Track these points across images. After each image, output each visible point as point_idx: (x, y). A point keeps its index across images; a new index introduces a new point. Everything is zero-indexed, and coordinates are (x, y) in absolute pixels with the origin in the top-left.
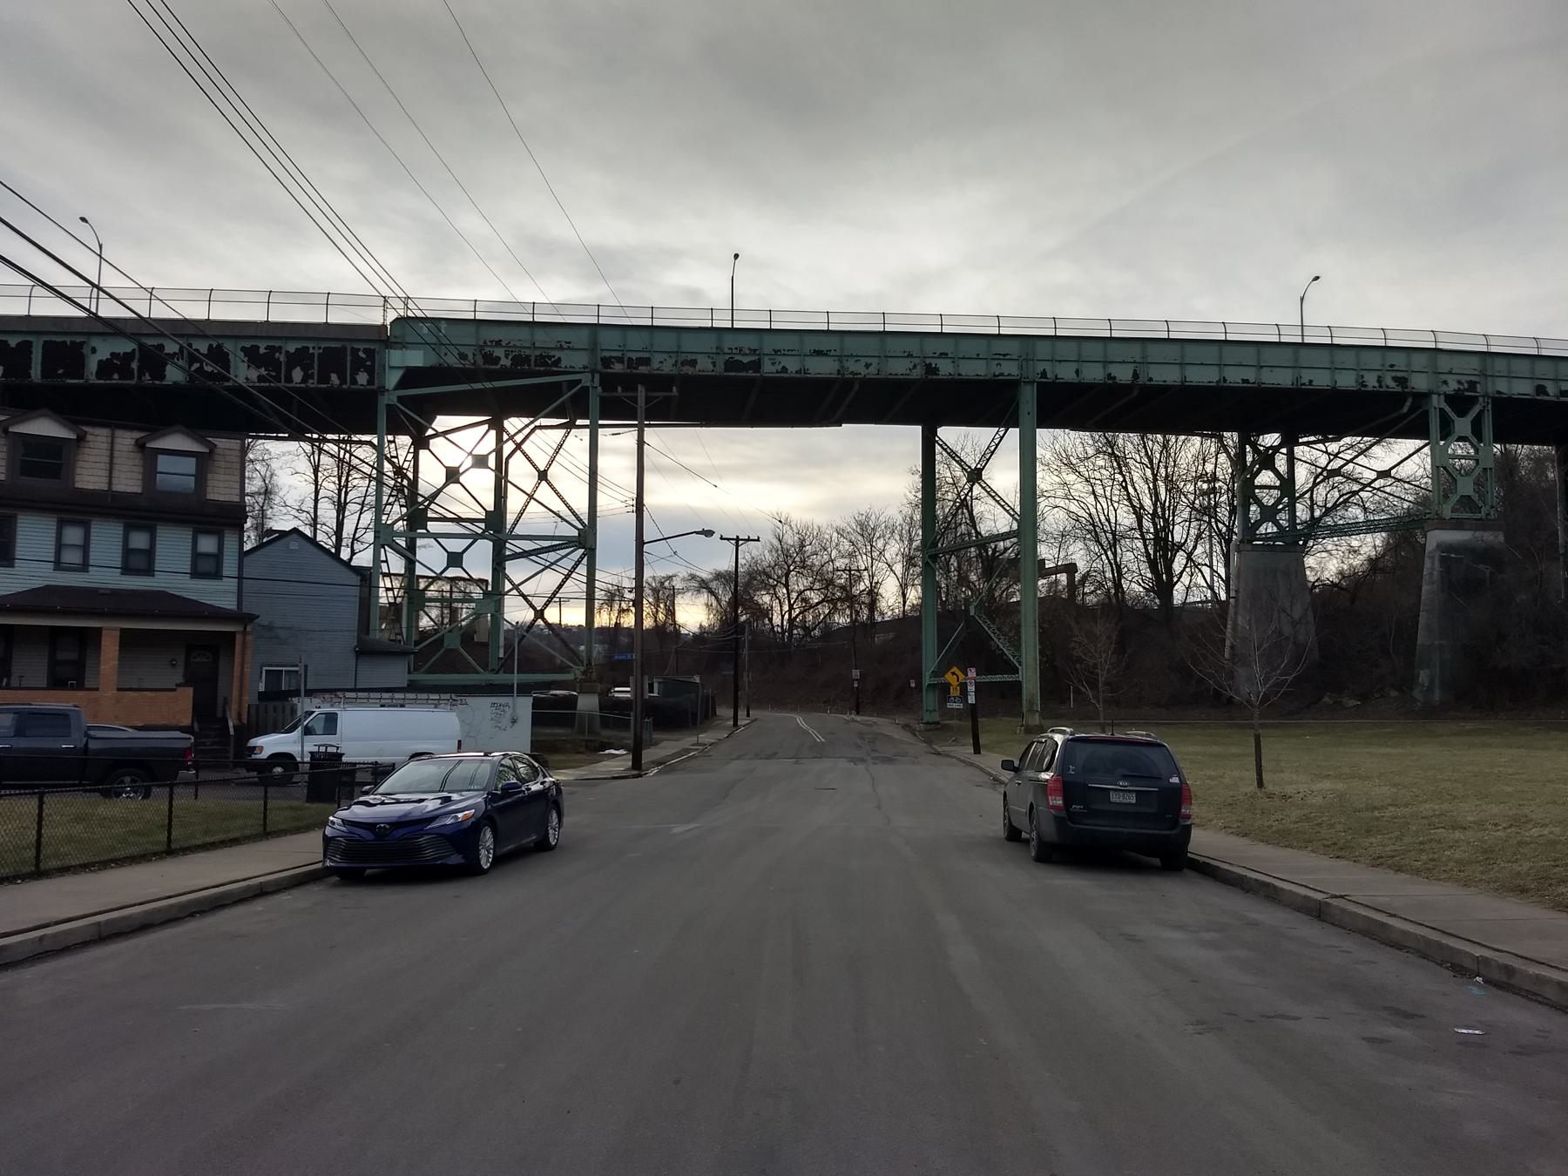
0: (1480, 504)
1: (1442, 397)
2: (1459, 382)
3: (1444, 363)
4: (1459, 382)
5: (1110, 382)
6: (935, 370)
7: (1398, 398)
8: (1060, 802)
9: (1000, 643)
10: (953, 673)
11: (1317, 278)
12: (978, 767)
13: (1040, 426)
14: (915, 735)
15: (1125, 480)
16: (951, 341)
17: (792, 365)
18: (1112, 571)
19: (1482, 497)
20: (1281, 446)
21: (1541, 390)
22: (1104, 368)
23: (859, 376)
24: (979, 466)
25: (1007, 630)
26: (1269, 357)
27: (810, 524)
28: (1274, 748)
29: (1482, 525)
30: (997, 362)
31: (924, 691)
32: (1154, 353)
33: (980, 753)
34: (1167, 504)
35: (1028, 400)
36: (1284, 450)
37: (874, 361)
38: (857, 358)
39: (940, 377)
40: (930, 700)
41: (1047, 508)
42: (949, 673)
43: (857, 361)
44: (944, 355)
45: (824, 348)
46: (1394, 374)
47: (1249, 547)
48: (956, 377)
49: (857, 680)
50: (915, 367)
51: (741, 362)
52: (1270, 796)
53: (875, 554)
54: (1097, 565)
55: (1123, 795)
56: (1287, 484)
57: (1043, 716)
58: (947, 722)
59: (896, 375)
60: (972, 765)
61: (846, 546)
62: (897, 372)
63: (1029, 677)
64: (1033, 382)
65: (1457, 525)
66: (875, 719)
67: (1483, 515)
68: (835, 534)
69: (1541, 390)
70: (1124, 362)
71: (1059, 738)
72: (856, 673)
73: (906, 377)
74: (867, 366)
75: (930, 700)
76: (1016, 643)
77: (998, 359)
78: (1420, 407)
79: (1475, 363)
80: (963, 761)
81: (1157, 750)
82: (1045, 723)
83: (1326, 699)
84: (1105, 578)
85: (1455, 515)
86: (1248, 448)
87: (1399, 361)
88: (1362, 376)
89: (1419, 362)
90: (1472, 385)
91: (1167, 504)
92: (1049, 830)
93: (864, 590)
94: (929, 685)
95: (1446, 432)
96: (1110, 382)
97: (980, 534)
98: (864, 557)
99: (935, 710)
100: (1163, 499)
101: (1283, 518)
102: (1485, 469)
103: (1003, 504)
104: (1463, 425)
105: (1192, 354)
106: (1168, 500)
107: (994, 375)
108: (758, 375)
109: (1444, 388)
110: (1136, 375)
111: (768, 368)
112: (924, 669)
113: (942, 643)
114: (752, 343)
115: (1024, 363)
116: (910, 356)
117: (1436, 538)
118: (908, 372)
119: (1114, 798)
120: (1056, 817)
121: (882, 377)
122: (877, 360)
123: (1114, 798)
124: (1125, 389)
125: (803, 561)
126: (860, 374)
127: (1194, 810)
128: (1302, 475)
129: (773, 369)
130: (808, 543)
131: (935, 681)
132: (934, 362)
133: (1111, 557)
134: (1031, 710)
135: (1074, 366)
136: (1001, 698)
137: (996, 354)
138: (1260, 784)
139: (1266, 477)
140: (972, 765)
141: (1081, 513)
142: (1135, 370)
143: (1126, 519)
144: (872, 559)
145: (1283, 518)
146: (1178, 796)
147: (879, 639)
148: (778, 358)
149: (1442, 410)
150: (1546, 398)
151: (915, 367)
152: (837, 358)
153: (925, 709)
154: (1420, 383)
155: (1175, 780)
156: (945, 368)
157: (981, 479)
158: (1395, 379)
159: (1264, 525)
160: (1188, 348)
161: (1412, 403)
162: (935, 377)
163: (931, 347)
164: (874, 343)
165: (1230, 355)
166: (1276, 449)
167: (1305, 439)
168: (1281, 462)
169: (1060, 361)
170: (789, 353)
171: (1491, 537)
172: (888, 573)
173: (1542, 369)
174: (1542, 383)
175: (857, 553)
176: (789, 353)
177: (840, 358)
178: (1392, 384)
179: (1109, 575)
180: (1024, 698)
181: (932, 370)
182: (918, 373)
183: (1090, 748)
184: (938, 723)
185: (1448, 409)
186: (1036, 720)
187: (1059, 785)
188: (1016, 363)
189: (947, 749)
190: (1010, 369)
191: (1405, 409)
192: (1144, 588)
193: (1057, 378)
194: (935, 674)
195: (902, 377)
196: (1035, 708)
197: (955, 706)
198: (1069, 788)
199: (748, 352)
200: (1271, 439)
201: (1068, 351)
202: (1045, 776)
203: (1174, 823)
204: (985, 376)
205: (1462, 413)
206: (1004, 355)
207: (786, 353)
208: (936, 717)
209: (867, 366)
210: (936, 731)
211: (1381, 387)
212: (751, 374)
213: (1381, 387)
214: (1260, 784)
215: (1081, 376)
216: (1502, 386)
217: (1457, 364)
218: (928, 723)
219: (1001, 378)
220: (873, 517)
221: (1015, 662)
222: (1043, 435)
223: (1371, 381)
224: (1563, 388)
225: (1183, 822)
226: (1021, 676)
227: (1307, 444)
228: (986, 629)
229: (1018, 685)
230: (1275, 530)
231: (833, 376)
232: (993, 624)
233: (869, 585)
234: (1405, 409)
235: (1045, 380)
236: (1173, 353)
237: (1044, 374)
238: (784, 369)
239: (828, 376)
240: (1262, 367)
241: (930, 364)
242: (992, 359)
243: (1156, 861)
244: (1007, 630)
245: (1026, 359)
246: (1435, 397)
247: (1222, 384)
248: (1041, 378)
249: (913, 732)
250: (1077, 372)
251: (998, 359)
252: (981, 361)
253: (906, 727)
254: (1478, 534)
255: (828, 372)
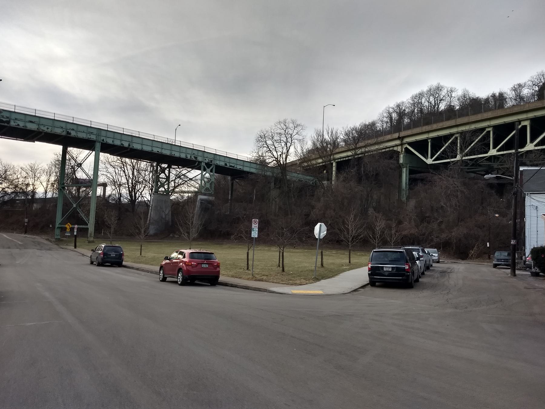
0: (210, 190)
1: (204, 163)
2: (209, 160)
3: (206, 155)
4: (209, 160)
5: (122, 146)
6: (70, 134)
7: (195, 162)
8: (102, 256)
9: (82, 215)
10: (68, 225)
11: (180, 125)
12: (77, 252)
13: (101, 152)
14: (52, 242)
15: (125, 170)
16: (76, 126)
17: (21, 124)
18: (118, 195)
19: (211, 188)
20: (167, 168)
21: (226, 164)
22: (121, 141)
23: (44, 131)
24: (81, 163)
25: (85, 211)
26: (165, 146)
27: (10, 164)
28: (326, 253)
29: (210, 195)
30: (90, 134)
31: (56, 228)
32: (135, 140)
33: (76, 248)
34: (137, 177)
35: (98, 146)
36: (168, 169)
37: (50, 128)
38: (44, 126)
39: (71, 136)
40: (57, 232)
41: (100, 175)
42: (67, 225)
43: (44, 126)
44: (73, 129)
45: (33, 121)
46: (194, 156)
47: (156, 194)
48: (77, 137)
49: (26, 222)
50: (63, 131)
51: (3, 120)
52: (142, 256)
53: (36, 179)
54: (114, 192)
55: (113, 255)
56: (168, 178)
57: (94, 238)
58: (63, 239)
59: (57, 133)
60: (75, 251)
61: (24, 174)
62: (57, 132)
63: (91, 227)
64: (100, 142)
65: (205, 195)
66: (35, 237)
67: (210, 193)
68: (20, 170)
69: (226, 164)
70: (126, 141)
71: (103, 246)
72: (26, 220)
73: (60, 134)
74: (48, 129)
75: (57, 232)
76: (88, 215)
77: (90, 134)
78: (199, 165)
79: (213, 156)
80: (72, 250)
81: (120, 248)
82: (94, 240)
83: (171, 235)
84: (116, 197)
85: (205, 192)
86: (159, 167)
87: (196, 152)
88: (187, 155)
89: (200, 154)
90: (211, 161)
91: (137, 177)
92: (100, 260)
93: (30, 190)
94: (58, 227)
95: (205, 170)
96: (122, 146)
97: (77, 177)
98: (32, 179)
99: (59, 235)
100: (136, 174)
101: (166, 187)
102: (212, 182)
103: (85, 172)
104: (209, 170)
105: (145, 142)
106: (137, 176)
107: (88, 138)
108: (9, 125)
109: (205, 161)
110: (129, 145)
111: (12, 124)
112: (56, 222)
113: (63, 215)
114: (8, 115)
115: (98, 136)
116: (62, 128)
117: (200, 197)
118: (61, 133)
119: (112, 255)
120: (102, 258)
121: (53, 133)
122: (51, 127)
123: (112, 255)
124: (126, 148)
125: (5, 177)
126: (45, 131)
127: (124, 258)
128: (172, 177)
129: (14, 124)
130: (8, 170)
131: (60, 226)
132: (70, 131)
133: (118, 191)
134: (91, 236)
135: (112, 140)
136: (83, 232)
137: (89, 132)
138: (141, 254)
139: (162, 175)
140: (75, 251)
141: (111, 177)
142: (129, 144)
143: (124, 180)
144: (35, 180)
145: (166, 187)
146: (122, 255)
147: (35, 206)
148: (16, 121)
149: (204, 166)
150: (226, 167)
151: (63, 131)
152: (37, 125)
153: (56, 234)
154: (200, 159)
155: (122, 252)
156: (73, 134)
157: (81, 166)
158: (194, 157)
159: (161, 188)
160: (144, 140)
161: (198, 163)
162: (70, 136)
163: (69, 126)
164: (51, 122)
165: (155, 144)
166: (166, 169)
167: (173, 167)
168: (167, 172)
169: (108, 137)
170: (21, 120)
171: (211, 198)
172: (40, 185)
173: (227, 160)
174: (226, 163)
175: (29, 177)
176: (21, 120)
177: (38, 125)
178: (194, 158)
179: (117, 196)
180: (89, 233)
181: (68, 133)
182: (64, 134)
183: (109, 247)
184: (60, 239)
185: (205, 166)
186: (92, 239)
187: (103, 253)
188: (95, 136)
189: (64, 247)
190: (93, 137)
191: (196, 165)
192: (128, 200)
193: (107, 142)
194: (60, 224)
195: (59, 134)
196: (92, 236)
197: (68, 234)
198: (104, 254)
199: (5, 117)
200: (165, 166)
201: (111, 135)
202: (100, 252)
203: (121, 259)
204: (86, 138)
205: (208, 168)
206: (92, 133)
207: (20, 120)
208: (59, 237)
209: (48, 129)
210: (59, 242)
211: (191, 158)
212: (6, 124)
213: (191, 158)
214: (141, 254)
215: (114, 143)
216: (218, 162)
217: (209, 156)
218: (56, 239)
219: (90, 139)
220: (36, 165)
221: (87, 222)
222: (101, 154)
223: (189, 157)
224: (231, 165)
225: (122, 259)
226: (88, 226)
227: (174, 168)
228: (79, 212)
229: (88, 228)
230: (164, 190)
231: (35, 130)
232: (80, 209)
233: (32, 189)
234: (196, 165)
235: (103, 142)
236: (140, 141)
237: (103, 140)
238: (18, 125)
239: (34, 129)
240: (163, 149)
241: (68, 131)
242: (88, 133)
243: (118, 266)
244: (85, 211)
245: (98, 135)
246: (203, 163)
247: (152, 151)
248: (102, 141)
249: (51, 241)
250: (113, 141)
251: (90, 134)
252: (85, 133)
253: (47, 240)
254: (209, 197)
255: (34, 128)
